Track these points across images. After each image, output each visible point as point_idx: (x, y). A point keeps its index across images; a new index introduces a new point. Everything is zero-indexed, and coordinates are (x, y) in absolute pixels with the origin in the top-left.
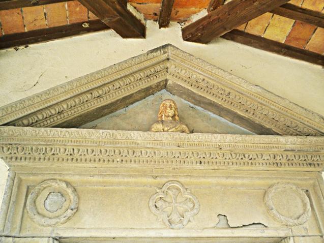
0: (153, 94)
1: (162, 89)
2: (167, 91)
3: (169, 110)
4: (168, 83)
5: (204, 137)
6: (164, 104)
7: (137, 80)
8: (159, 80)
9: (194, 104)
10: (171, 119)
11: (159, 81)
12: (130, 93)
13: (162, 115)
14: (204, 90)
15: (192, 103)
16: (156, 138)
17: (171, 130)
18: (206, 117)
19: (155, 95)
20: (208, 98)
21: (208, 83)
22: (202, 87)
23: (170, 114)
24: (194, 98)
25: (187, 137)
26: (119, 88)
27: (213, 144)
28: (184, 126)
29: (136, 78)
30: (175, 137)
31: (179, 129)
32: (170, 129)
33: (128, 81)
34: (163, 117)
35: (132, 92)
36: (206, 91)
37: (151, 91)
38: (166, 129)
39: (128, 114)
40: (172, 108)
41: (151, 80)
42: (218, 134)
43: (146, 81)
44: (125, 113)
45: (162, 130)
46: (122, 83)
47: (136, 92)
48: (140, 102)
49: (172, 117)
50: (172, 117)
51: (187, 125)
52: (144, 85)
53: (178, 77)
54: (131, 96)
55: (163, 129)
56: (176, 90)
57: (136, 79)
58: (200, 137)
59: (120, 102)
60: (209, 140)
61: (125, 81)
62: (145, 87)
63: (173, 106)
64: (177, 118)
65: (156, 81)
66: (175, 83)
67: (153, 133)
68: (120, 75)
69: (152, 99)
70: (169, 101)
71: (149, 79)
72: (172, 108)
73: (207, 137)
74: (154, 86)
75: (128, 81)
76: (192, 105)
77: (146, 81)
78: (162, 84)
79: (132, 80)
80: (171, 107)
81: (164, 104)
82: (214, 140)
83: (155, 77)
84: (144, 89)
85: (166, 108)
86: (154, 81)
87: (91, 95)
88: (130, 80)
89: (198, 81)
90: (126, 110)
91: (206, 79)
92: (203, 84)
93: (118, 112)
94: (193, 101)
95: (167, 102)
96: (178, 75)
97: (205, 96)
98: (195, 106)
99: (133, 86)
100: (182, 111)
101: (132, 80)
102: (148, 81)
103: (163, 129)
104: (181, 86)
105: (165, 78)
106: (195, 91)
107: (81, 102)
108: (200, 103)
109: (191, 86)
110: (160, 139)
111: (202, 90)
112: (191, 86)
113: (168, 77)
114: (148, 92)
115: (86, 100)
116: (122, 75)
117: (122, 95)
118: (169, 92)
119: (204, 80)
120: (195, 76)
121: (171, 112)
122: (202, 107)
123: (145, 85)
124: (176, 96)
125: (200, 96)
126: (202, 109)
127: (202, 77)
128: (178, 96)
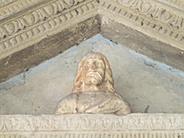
0: (77, 44)
1: (94, 34)
2: (104, 36)
3: (91, 72)
4: (103, 23)
5: (149, 121)
6: (84, 62)
7: (39, 21)
8: (82, 17)
9: (154, 59)
10: (96, 88)
11: (83, 20)
12: (26, 46)
13: (81, 83)
14: (166, 30)
15: (149, 56)
16: (57, 127)
17: (89, 111)
18: (174, 82)
19: (81, 45)
20: (173, 45)
21: (171, 16)
22: (162, 25)
23: (92, 80)
24: (150, 48)
25: (116, 122)
26: (5, 36)
27: (167, 133)
28: (120, 102)
29: (36, 17)
30: (93, 123)
31: (107, 107)
32: (88, 109)
33: (21, 23)
34: (83, 86)
35: (31, 43)
36: (169, 32)
37: (72, 38)
38: (82, 108)
39: (27, 84)
40: (97, 67)
41: (66, 19)
42: (176, 115)
43: (57, 20)
44: (22, 81)
45: (75, 111)
46: (8, 28)
47: (39, 43)
48: (52, 60)
49: (98, 85)
50: (98, 85)
51: (125, 100)
52: (53, 28)
53: (118, 10)
54: (30, 50)
55: (77, 109)
56: (118, 33)
57: (36, 19)
58: (142, 122)
59: (10, 63)
60: (159, 126)
61: (15, 23)
62: (55, 32)
63: (99, 65)
64: (109, 86)
65: (77, 21)
66: (113, 21)
67: (62, 117)
68: (5, 13)
69: (75, 53)
70: (94, 56)
71: (62, 18)
72: (97, 67)
73: (154, 121)
74: (73, 30)
75: (21, 23)
76: (149, 60)
77: (57, 20)
78: (90, 24)
79: (29, 21)
80: (95, 65)
81: (84, 62)
82: (168, 125)
83: (74, 13)
84: (54, 36)
85: (87, 69)
86: (73, 21)
87: (31, 16)
88: (25, 21)
89: (153, 14)
90: (24, 76)
91: (168, 9)
92: (162, 20)
93: (10, 81)
94: (151, 53)
95: (84, 62)
96: (118, 6)
97: (167, 43)
98: (157, 63)
99: (32, 33)
100: (129, 73)
101: (29, 21)
102: (61, 21)
103: (77, 109)
104: (124, 26)
105: (95, 14)
106: (148, 34)
107: (16, 30)
108: (163, 57)
109: (142, 24)
110: (65, 128)
111: (161, 32)
112: (142, 24)
113: (99, 12)
114: (63, 41)
115: (44, 16)
116: (8, 14)
117: (11, 50)
118: (108, 38)
119: (163, 12)
120: (147, 6)
121: (94, 76)
122: (168, 64)
123: (32, 40)
124: (119, 45)
125: (159, 42)
126: (169, 67)
127: (160, 7)
128: (123, 44)
